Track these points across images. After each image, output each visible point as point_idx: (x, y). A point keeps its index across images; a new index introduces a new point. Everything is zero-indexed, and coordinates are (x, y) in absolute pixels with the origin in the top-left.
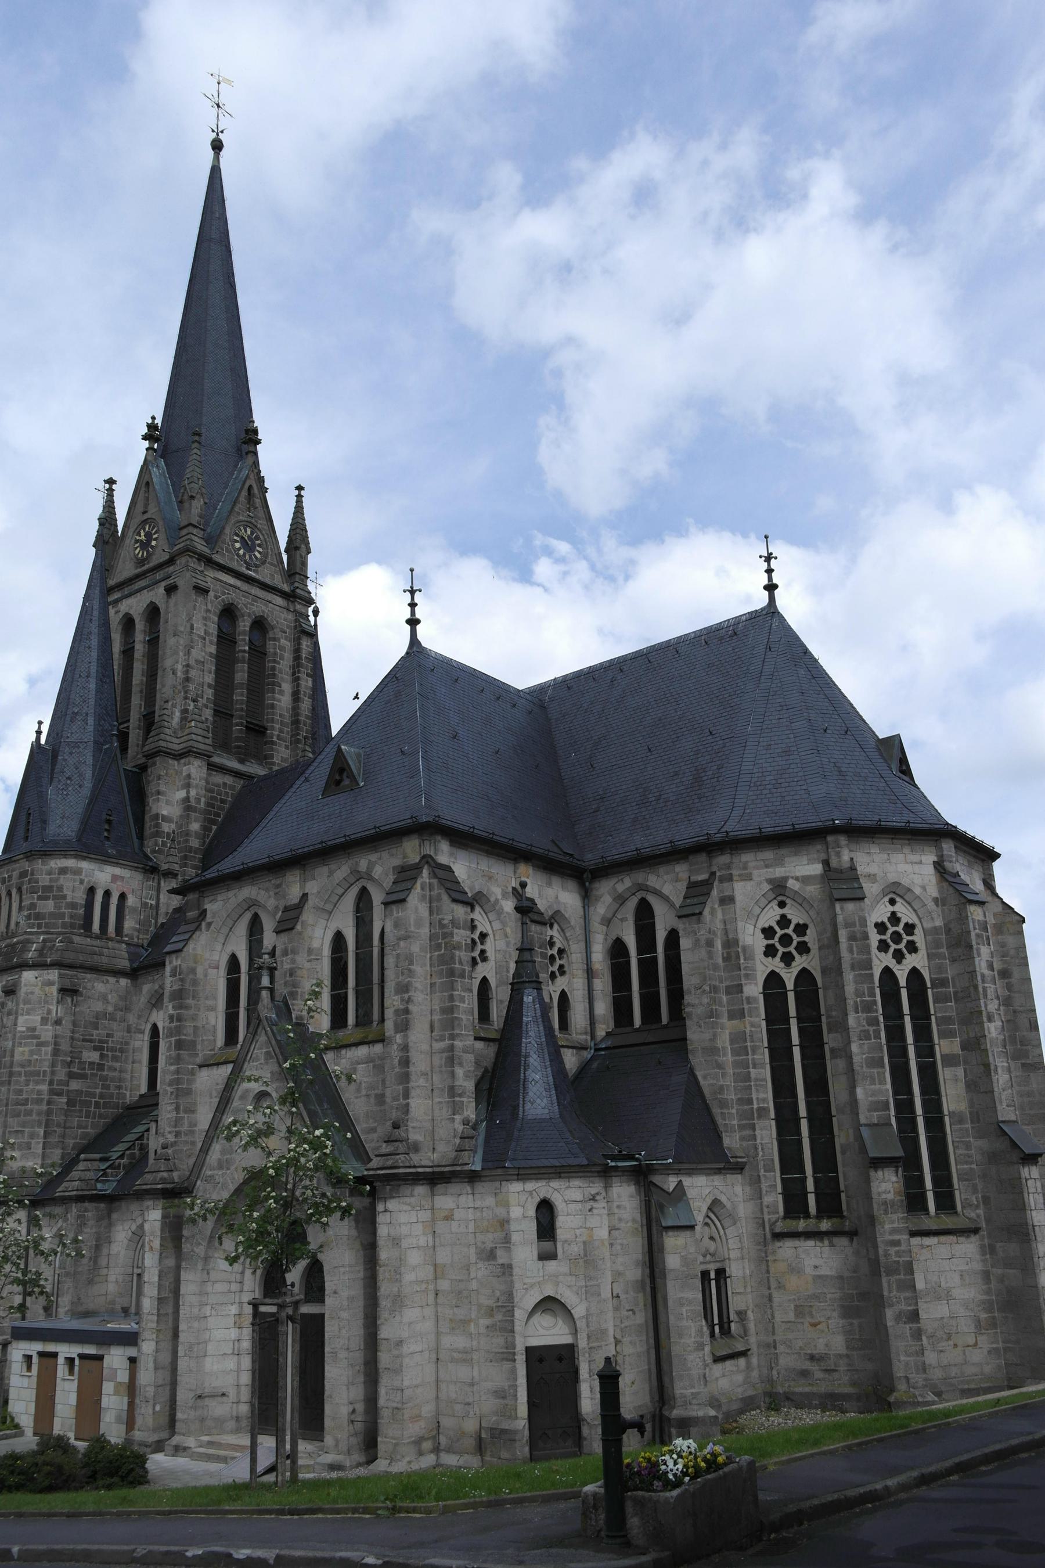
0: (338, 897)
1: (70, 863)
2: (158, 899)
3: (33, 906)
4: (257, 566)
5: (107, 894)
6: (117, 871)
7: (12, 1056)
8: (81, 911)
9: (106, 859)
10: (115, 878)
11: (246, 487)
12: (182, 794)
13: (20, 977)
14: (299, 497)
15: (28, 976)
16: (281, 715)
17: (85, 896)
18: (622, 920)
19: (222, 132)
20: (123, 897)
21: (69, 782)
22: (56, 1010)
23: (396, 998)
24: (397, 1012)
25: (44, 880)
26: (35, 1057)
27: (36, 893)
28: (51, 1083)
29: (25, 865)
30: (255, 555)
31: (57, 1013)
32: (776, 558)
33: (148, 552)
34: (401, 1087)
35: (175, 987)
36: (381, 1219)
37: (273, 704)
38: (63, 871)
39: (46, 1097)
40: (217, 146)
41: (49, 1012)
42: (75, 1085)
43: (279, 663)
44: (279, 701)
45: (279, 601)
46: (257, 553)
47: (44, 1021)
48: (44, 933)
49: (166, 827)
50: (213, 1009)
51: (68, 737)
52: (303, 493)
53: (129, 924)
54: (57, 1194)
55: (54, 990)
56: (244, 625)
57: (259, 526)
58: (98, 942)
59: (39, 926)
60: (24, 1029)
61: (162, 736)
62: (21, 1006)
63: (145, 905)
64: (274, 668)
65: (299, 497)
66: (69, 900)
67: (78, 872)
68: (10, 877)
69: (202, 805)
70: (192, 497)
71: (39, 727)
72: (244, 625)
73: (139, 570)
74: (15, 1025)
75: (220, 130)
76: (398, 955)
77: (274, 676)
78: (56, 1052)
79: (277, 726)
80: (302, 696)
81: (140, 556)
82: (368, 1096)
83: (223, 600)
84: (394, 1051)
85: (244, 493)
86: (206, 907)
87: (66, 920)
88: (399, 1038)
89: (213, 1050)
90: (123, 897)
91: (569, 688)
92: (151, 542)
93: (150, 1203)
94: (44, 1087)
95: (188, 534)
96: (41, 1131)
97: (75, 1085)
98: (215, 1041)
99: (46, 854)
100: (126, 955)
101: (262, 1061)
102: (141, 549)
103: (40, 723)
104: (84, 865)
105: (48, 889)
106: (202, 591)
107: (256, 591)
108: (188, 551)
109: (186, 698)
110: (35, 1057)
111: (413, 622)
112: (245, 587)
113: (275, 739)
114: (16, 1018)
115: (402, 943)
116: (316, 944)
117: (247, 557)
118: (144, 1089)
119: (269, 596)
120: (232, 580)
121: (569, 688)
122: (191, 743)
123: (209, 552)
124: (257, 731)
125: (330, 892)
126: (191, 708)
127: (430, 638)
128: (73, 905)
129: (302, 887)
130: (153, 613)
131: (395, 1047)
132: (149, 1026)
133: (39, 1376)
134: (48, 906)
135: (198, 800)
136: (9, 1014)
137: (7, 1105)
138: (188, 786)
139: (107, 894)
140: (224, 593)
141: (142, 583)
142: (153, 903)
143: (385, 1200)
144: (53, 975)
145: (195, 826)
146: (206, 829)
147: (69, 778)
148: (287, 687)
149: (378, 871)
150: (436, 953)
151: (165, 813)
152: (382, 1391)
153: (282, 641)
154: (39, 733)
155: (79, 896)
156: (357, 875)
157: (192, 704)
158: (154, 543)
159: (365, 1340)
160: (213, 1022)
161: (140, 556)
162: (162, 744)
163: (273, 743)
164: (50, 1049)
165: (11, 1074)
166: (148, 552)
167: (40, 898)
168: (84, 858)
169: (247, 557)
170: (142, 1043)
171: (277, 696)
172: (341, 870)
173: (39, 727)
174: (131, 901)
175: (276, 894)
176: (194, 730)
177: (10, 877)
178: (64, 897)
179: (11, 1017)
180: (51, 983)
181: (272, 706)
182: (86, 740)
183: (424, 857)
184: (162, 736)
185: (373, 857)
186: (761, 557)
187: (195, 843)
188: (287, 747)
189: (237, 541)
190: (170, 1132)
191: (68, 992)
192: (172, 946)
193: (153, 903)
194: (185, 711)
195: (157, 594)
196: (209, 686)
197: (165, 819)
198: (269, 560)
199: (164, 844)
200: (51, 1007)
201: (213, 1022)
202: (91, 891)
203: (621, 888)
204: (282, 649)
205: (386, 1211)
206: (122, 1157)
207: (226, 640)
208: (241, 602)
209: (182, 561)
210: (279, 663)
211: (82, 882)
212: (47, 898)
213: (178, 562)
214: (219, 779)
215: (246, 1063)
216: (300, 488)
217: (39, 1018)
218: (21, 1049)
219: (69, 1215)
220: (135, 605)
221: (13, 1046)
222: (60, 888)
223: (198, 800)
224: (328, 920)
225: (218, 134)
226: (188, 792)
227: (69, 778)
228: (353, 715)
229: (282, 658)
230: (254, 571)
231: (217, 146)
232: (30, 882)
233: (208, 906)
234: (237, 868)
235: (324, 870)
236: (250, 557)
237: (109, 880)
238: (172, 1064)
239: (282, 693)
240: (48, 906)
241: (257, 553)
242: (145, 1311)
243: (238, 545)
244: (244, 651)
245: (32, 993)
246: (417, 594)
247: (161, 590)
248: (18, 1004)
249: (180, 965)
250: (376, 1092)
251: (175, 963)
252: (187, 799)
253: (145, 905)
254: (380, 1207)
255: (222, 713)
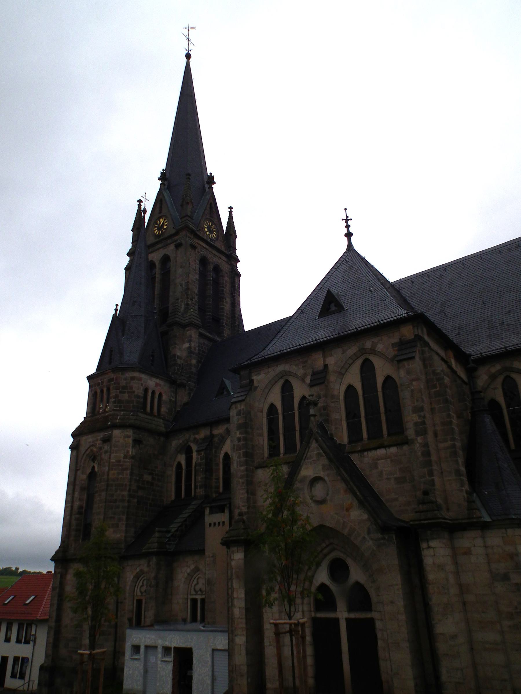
0: (349, 365)
1: (137, 374)
2: (176, 398)
3: (117, 396)
4: (215, 241)
5: (153, 392)
6: (158, 381)
7: (108, 475)
8: (142, 400)
9: (153, 374)
10: (157, 385)
11: (209, 203)
12: (187, 345)
13: (112, 433)
14: (231, 213)
15: (117, 432)
16: (227, 314)
17: (143, 392)
18: (494, 389)
19: (190, 51)
20: (160, 395)
21: (132, 335)
22: (131, 451)
23: (414, 415)
24: (416, 424)
25: (123, 383)
26: (121, 476)
27: (119, 389)
28: (129, 491)
29: (112, 375)
30: (213, 235)
31: (132, 453)
32: (351, 219)
33: (162, 231)
34: (426, 470)
35: (240, 422)
36: (425, 553)
37: (223, 307)
38: (133, 378)
39: (127, 499)
40: (188, 56)
41: (128, 452)
42: (140, 493)
43: (225, 288)
44: (225, 306)
45: (224, 258)
46: (214, 235)
47: (125, 457)
48: (123, 410)
49: (179, 362)
50: (261, 435)
51: (131, 313)
52: (232, 210)
53: (164, 409)
54: (144, 551)
55: (130, 440)
56: (211, 267)
57: (215, 222)
58: (149, 417)
59: (120, 407)
60: (114, 461)
61: (177, 316)
62: (113, 448)
63: (170, 400)
64: (223, 290)
65: (231, 213)
66: (136, 393)
67: (140, 379)
68: (102, 382)
69: (197, 351)
70: (188, 203)
71: (117, 307)
72: (211, 267)
73: (157, 240)
74: (110, 458)
75: (189, 50)
76: (412, 391)
77: (223, 294)
78: (132, 474)
79: (225, 318)
80: (236, 305)
81: (157, 233)
82: (388, 479)
83: (201, 254)
84: (417, 447)
85: (208, 206)
86: (253, 378)
87: (135, 404)
88: (420, 440)
89: (263, 458)
90: (160, 395)
91: (412, 282)
92: (164, 226)
93: (235, 549)
94: (126, 493)
95: (186, 220)
96: (124, 517)
97: (140, 493)
98: (263, 454)
99: (124, 370)
100: (163, 425)
101: (315, 458)
102: (158, 230)
103: (117, 305)
104: (143, 376)
105: (124, 387)
106: (194, 247)
107: (214, 252)
108: (187, 228)
109: (188, 298)
110: (121, 476)
111: (349, 235)
112: (210, 249)
113: (224, 324)
114: (110, 455)
115: (414, 383)
116: (336, 393)
117: (210, 236)
118: (173, 497)
119: (220, 256)
120: (205, 245)
121: (412, 282)
122: (192, 319)
123: (196, 230)
124: (217, 320)
125: (344, 362)
126: (190, 303)
127: (145, 207)
128: (138, 397)
129: (324, 361)
130: (166, 259)
131: (418, 445)
132: (175, 464)
133: (174, 656)
134: (125, 396)
135: (195, 349)
136: (106, 452)
137: (105, 502)
138: (190, 341)
139: (153, 392)
140: (202, 251)
141: (160, 246)
142: (174, 399)
143: (428, 541)
144: (130, 432)
145: (194, 362)
146: (199, 362)
147: (133, 333)
148: (228, 300)
149: (380, 347)
150: (433, 390)
151: (178, 354)
152: (444, 671)
153: (226, 278)
154: (116, 310)
155: (140, 392)
156: (363, 351)
157: (190, 301)
158: (165, 227)
159: (167, 647)
160: (262, 443)
161: (215, 236)
162: (177, 319)
163: (223, 326)
164: (129, 472)
165: (108, 485)
166: (162, 231)
167: (120, 392)
168: (144, 373)
169: (210, 236)
170: (172, 472)
171: (225, 304)
172: (352, 350)
173: (117, 307)
174: (164, 397)
175: (303, 367)
176: (193, 313)
177: (102, 382)
178: (134, 392)
179: (107, 454)
180: (128, 437)
181: (223, 309)
182: (140, 315)
183: (416, 336)
184: (177, 316)
185: (376, 340)
186: (343, 220)
187: (194, 370)
188: (229, 329)
189: (206, 228)
190: (243, 506)
191: (137, 442)
192: (235, 399)
193: (174, 399)
194: (187, 304)
195: (170, 250)
196: (197, 295)
197: (179, 357)
198: (219, 238)
199: (178, 369)
200: (129, 449)
201: (262, 443)
202: (146, 390)
203: (493, 370)
204: (226, 281)
205: (429, 547)
206: (177, 531)
207: (203, 274)
208: (209, 256)
209: (183, 234)
210: (225, 288)
211: (142, 385)
212: (124, 392)
213: (181, 234)
214: (202, 341)
215: (303, 461)
216: (231, 208)
217: (122, 455)
218: (113, 472)
219: (151, 563)
220: (156, 257)
221: (109, 470)
222: (131, 388)
223: (195, 349)
224: (342, 379)
225: (188, 51)
226: (190, 344)
227: (133, 333)
228: (322, 281)
229: (226, 286)
230: (214, 243)
231: (188, 56)
232: (115, 383)
233: (254, 378)
234: (277, 353)
235: (339, 351)
236: (211, 236)
237: (154, 385)
238: (242, 466)
239: (226, 302)
240: (125, 396)
241: (214, 235)
242: (236, 616)
243: (206, 230)
244: (210, 280)
245: (118, 441)
246: (349, 221)
247: (172, 247)
248: (111, 448)
249: (243, 409)
250: (395, 476)
251: (239, 408)
252: (190, 347)
253: (170, 400)
254: (424, 545)
255: (202, 310)
